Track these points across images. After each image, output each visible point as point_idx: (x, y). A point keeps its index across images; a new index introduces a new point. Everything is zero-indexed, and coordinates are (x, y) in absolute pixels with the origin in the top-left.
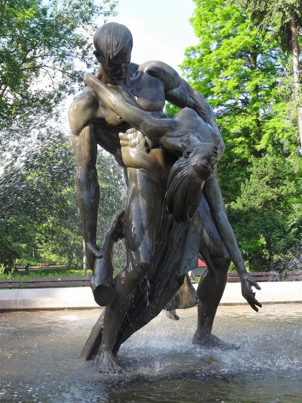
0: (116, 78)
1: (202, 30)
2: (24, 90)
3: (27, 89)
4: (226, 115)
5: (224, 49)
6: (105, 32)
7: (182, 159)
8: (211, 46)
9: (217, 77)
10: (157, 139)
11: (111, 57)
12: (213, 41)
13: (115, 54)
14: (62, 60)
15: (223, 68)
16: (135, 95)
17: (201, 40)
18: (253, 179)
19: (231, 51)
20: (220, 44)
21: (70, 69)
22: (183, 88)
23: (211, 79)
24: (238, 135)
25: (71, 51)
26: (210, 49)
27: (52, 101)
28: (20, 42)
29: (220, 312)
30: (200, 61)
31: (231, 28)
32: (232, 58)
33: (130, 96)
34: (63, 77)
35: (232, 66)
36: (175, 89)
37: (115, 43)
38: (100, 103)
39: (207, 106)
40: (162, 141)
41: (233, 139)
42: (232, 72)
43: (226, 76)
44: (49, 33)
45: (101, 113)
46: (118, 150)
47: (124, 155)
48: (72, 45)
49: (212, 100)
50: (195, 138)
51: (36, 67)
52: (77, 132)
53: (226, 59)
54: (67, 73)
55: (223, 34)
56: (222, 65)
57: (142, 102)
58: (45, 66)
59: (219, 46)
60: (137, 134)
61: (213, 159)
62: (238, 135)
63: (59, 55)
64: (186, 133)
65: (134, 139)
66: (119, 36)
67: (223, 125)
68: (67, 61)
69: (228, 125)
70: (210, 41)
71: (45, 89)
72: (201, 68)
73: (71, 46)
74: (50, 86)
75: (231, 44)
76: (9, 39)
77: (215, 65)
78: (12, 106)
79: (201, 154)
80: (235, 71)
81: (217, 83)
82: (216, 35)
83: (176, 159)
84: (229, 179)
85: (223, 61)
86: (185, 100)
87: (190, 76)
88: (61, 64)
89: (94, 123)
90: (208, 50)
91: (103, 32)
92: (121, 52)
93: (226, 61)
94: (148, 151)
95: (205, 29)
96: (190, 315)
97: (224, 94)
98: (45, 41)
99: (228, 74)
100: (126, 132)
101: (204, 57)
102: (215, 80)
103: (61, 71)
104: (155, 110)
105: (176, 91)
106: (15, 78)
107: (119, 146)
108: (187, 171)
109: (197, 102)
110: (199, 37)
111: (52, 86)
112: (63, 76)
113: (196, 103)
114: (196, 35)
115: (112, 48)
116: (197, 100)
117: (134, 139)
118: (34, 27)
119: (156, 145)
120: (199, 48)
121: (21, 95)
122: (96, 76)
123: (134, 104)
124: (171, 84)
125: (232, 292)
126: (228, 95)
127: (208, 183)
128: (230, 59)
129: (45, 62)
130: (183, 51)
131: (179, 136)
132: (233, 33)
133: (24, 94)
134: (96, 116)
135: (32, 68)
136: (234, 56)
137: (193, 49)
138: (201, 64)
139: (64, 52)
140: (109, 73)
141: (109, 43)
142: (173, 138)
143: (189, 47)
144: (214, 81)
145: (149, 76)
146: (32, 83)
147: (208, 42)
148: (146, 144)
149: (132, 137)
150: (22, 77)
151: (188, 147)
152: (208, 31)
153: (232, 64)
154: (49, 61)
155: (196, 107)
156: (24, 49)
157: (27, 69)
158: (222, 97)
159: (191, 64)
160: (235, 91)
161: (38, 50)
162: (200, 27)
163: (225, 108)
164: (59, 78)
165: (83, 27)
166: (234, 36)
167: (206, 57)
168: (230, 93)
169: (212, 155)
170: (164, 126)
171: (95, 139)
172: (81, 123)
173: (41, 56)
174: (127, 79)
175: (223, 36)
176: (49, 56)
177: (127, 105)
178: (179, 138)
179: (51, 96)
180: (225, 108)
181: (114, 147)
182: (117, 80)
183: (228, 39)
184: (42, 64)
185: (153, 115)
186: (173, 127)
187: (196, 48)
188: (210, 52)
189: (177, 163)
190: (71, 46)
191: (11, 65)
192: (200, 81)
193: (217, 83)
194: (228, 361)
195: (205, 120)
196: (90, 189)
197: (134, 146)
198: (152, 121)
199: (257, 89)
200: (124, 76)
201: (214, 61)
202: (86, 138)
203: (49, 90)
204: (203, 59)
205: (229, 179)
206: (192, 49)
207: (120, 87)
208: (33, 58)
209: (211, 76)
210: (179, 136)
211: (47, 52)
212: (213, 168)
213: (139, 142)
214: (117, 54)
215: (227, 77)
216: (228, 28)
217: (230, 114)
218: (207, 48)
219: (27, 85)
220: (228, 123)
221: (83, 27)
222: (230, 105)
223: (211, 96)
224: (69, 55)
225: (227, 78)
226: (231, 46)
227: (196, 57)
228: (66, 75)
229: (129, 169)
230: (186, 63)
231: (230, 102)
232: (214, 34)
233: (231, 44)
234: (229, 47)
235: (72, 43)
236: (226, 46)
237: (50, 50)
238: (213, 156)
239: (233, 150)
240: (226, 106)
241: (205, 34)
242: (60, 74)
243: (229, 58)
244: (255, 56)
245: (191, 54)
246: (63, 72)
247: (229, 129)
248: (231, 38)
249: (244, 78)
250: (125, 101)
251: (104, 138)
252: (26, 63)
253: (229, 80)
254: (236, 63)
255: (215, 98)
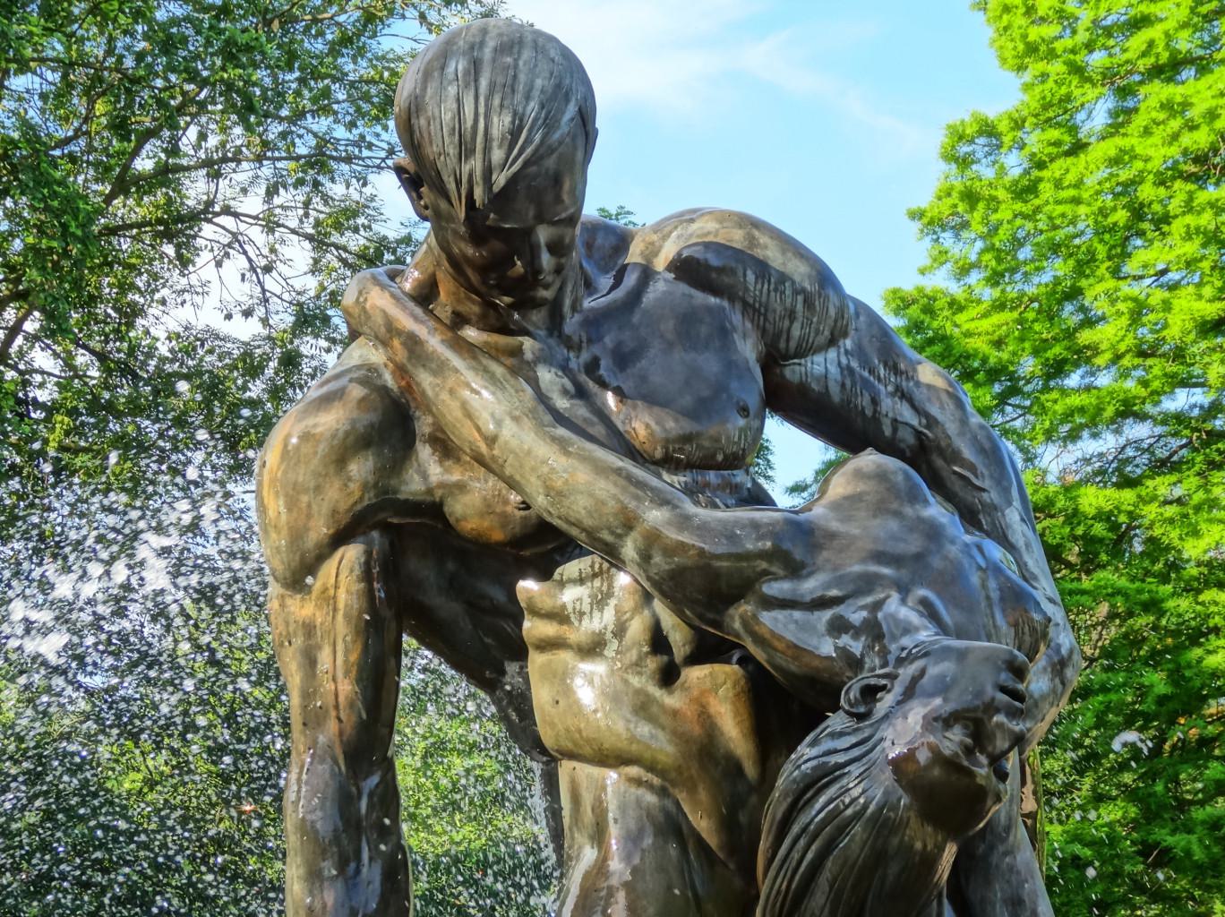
0: (507, 300)
1: (1035, 33)
2: (117, 331)
3: (130, 325)
4: (1163, 466)
5: (1147, 132)
6: (450, 69)
7: (836, 721)
8: (1081, 116)
9: (1116, 273)
10: (710, 616)
11: (478, 193)
12: (1091, 93)
13: (500, 180)
14: (316, 184)
15: (1146, 226)
16: (604, 385)
17: (1027, 87)
19: (1187, 140)
20: (1130, 104)
21: (356, 230)
22: (860, 353)
23: (1083, 283)
25: (362, 137)
26: (1073, 129)
27: (256, 389)
28: (99, 95)
30: (1026, 190)
31: (1184, 26)
32: (1188, 178)
33: (581, 393)
34: (315, 268)
35: (1190, 219)
36: (819, 358)
37: (501, 123)
38: (424, 425)
39: (987, 445)
40: (737, 625)
41: (1199, 592)
42: (1191, 248)
43: (1161, 266)
44: (248, 49)
45: (425, 476)
46: (512, 667)
47: (541, 696)
48: (365, 107)
49: (1088, 388)
50: (908, 614)
51: (180, 219)
53: (1161, 182)
54: (337, 247)
55: (1144, 54)
56: (1138, 212)
57: (642, 425)
58: (227, 211)
59: (1121, 118)
60: (610, 586)
61: (1000, 726)
63: (298, 158)
64: (867, 584)
65: (596, 614)
66: (521, 88)
67: (1146, 522)
68: (337, 190)
69: (1171, 521)
70: (1077, 92)
71: (225, 328)
72: (1029, 226)
73: (358, 109)
74: (247, 313)
75: (1186, 105)
76: (49, 75)
77: (1103, 212)
78: (51, 409)
79: (938, 701)
80: (1204, 246)
81: (1113, 302)
82: (1107, 62)
83: (813, 719)
84: (1183, 805)
85: (1147, 192)
86: (869, 412)
87: (973, 266)
88: (307, 204)
89: (385, 527)
90: (1067, 138)
91: (443, 68)
92: (533, 169)
93: (1162, 191)
94: (668, 676)
95: (1050, 30)
97: (1150, 362)
98: (230, 86)
99: (1172, 256)
100: (556, 576)
101: (1045, 174)
102: (1100, 288)
103: (310, 238)
104: (723, 466)
105: (823, 367)
106: (73, 271)
107: (519, 651)
108: (866, 789)
109: (932, 422)
110: (1021, 68)
111: (260, 312)
112: (316, 261)
113: (928, 427)
114: (1004, 60)
115: (487, 150)
116: (934, 410)
117: (596, 614)
118: (175, 21)
119: (709, 649)
120: (1018, 124)
121: (102, 357)
122: (408, 286)
123: (599, 430)
124: (796, 332)
126: (1173, 368)
127: (982, 848)
128: (1178, 184)
129: (225, 190)
130: (938, 139)
131: (821, 603)
132: (1201, 52)
133: (118, 350)
134: (396, 492)
135: (160, 221)
137: (988, 130)
138: (1026, 208)
139: (323, 141)
140: (470, 272)
141: (469, 123)
142: (797, 614)
143: (967, 119)
144: (1096, 291)
145: (683, 288)
146: (157, 296)
147: (1068, 98)
148: (658, 642)
149: (587, 600)
150: (110, 265)
151: (872, 661)
152: (1068, 42)
153: (1189, 207)
154: (244, 190)
155: (925, 456)
156: (120, 126)
157: (131, 226)
158: (1139, 373)
159: (981, 206)
160: (1204, 345)
161: (193, 132)
162: (1023, 21)
163: (1159, 430)
165: (423, 17)
166: (1202, 66)
167: (1056, 169)
168: (1179, 354)
169: (991, 708)
170: (750, 546)
171: (393, 612)
172: (320, 530)
173: (207, 163)
174: (567, 302)
175: (1142, 65)
176: (245, 165)
177: (554, 439)
178: (827, 615)
180: (1159, 430)
181: (490, 651)
182: (511, 306)
183: (1170, 80)
184: (210, 203)
185: (691, 491)
186: (798, 554)
187: (1003, 126)
188: (1078, 148)
189: (813, 744)
190: (358, 109)
191: (47, 209)
192: (1022, 294)
193: (1113, 302)
195: (970, 517)
196: (358, 871)
197: (593, 649)
198: (684, 521)
200: (547, 287)
201: (1098, 193)
202: (341, 605)
203: (245, 330)
204: (1040, 180)
205: (1183, 805)
206: (981, 133)
207: (528, 344)
208: (165, 175)
209: (1085, 265)
210: (821, 603)
211: (238, 142)
212: (1002, 776)
213: (620, 631)
214: (512, 182)
215: (1164, 272)
216: (1170, 25)
217: (1180, 462)
218: (1059, 125)
219: (133, 305)
220: (1171, 511)
221: (423, 17)
222: (1180, 418)
223: (1080, 372)
224: (348, 160)
225: (1164, 279)
226: (1189, 115)
227: (1002, 171)
228: (331, 258)
229: (565, 769)
230: (949, 201)
231: (1181, 400)
232: (1098, 59)
233: (1186, 105)
234: (1175, 124)
235: (367, 97)
236: (1162, 116)
237: (249, 128)
238: (998, 711)
239: (1197, 652)
240: (1164, 423)
241: (1052, 55)
242: (298, 254)
243: (1174, 178)
245: (980, 155)
246: (319, 242)
247: (1176, 542)
248: (1184, 75)
250: (548, 418)
251: (447, 607)
252: (127, 194)
253: (1173, 287)
254: (1212, 205)
255: (1104, 380)
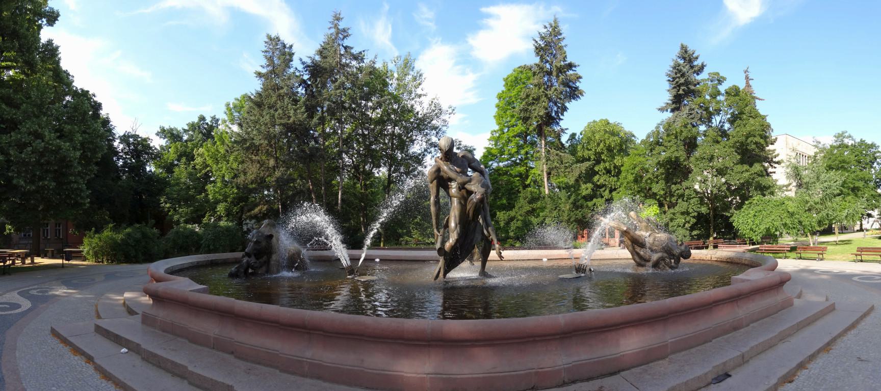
18: (521, 200)
24: (516, 176)
29: (488, 264)
52: (432, 182)
62: (516, 176)
96: (478, 264)
125: (493, 254)
136: (515, 136)
164: (424, 145)
179: (420, 155)
181: (447, 188)
194: (491, 281)
199: (527, 153)
203: (419, 152)
244: (526, 137)
249: (520, 147)
